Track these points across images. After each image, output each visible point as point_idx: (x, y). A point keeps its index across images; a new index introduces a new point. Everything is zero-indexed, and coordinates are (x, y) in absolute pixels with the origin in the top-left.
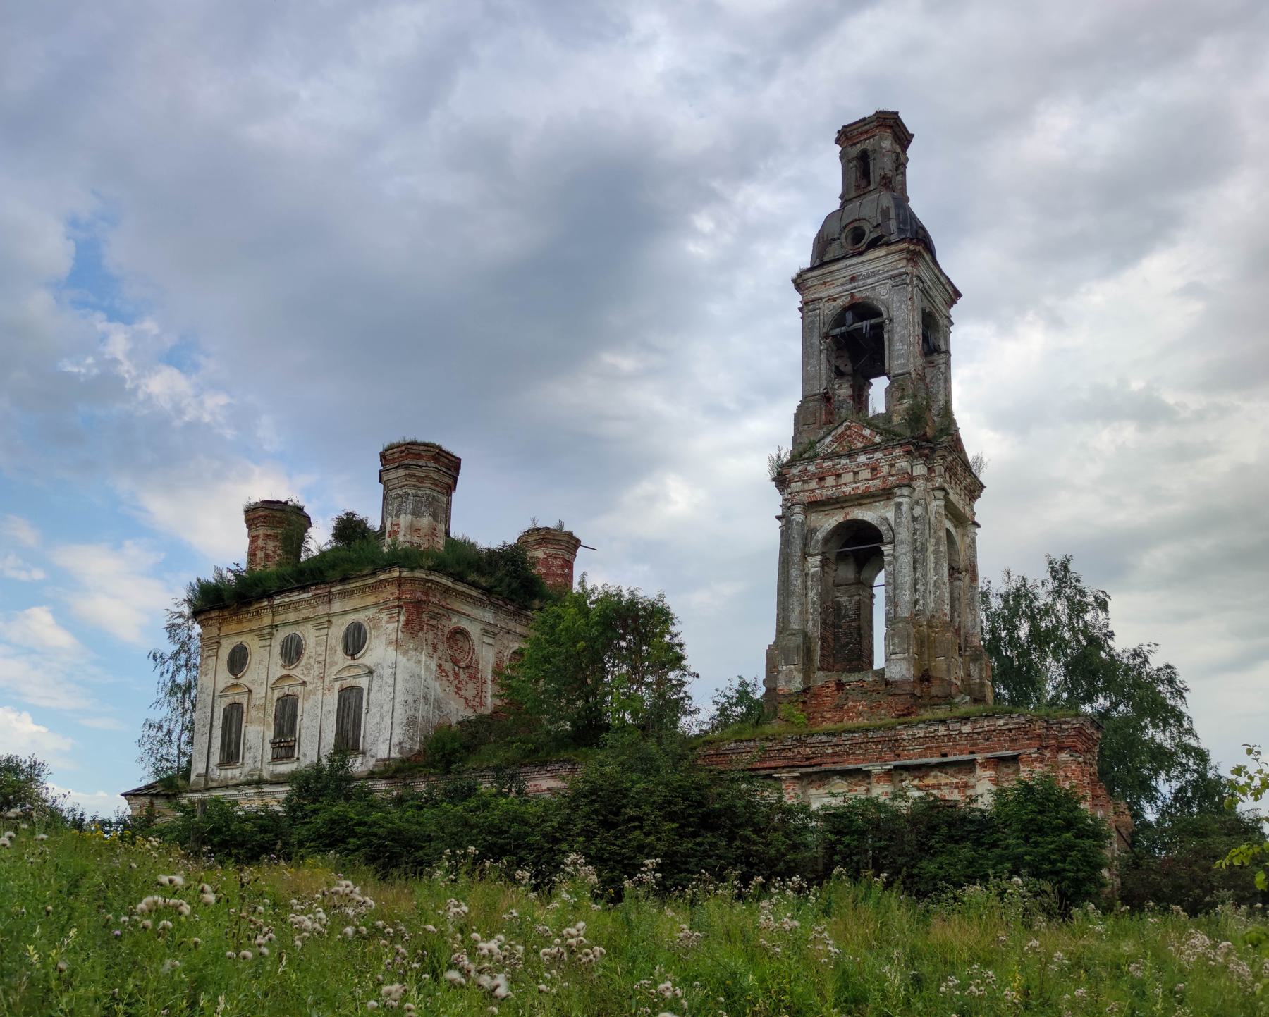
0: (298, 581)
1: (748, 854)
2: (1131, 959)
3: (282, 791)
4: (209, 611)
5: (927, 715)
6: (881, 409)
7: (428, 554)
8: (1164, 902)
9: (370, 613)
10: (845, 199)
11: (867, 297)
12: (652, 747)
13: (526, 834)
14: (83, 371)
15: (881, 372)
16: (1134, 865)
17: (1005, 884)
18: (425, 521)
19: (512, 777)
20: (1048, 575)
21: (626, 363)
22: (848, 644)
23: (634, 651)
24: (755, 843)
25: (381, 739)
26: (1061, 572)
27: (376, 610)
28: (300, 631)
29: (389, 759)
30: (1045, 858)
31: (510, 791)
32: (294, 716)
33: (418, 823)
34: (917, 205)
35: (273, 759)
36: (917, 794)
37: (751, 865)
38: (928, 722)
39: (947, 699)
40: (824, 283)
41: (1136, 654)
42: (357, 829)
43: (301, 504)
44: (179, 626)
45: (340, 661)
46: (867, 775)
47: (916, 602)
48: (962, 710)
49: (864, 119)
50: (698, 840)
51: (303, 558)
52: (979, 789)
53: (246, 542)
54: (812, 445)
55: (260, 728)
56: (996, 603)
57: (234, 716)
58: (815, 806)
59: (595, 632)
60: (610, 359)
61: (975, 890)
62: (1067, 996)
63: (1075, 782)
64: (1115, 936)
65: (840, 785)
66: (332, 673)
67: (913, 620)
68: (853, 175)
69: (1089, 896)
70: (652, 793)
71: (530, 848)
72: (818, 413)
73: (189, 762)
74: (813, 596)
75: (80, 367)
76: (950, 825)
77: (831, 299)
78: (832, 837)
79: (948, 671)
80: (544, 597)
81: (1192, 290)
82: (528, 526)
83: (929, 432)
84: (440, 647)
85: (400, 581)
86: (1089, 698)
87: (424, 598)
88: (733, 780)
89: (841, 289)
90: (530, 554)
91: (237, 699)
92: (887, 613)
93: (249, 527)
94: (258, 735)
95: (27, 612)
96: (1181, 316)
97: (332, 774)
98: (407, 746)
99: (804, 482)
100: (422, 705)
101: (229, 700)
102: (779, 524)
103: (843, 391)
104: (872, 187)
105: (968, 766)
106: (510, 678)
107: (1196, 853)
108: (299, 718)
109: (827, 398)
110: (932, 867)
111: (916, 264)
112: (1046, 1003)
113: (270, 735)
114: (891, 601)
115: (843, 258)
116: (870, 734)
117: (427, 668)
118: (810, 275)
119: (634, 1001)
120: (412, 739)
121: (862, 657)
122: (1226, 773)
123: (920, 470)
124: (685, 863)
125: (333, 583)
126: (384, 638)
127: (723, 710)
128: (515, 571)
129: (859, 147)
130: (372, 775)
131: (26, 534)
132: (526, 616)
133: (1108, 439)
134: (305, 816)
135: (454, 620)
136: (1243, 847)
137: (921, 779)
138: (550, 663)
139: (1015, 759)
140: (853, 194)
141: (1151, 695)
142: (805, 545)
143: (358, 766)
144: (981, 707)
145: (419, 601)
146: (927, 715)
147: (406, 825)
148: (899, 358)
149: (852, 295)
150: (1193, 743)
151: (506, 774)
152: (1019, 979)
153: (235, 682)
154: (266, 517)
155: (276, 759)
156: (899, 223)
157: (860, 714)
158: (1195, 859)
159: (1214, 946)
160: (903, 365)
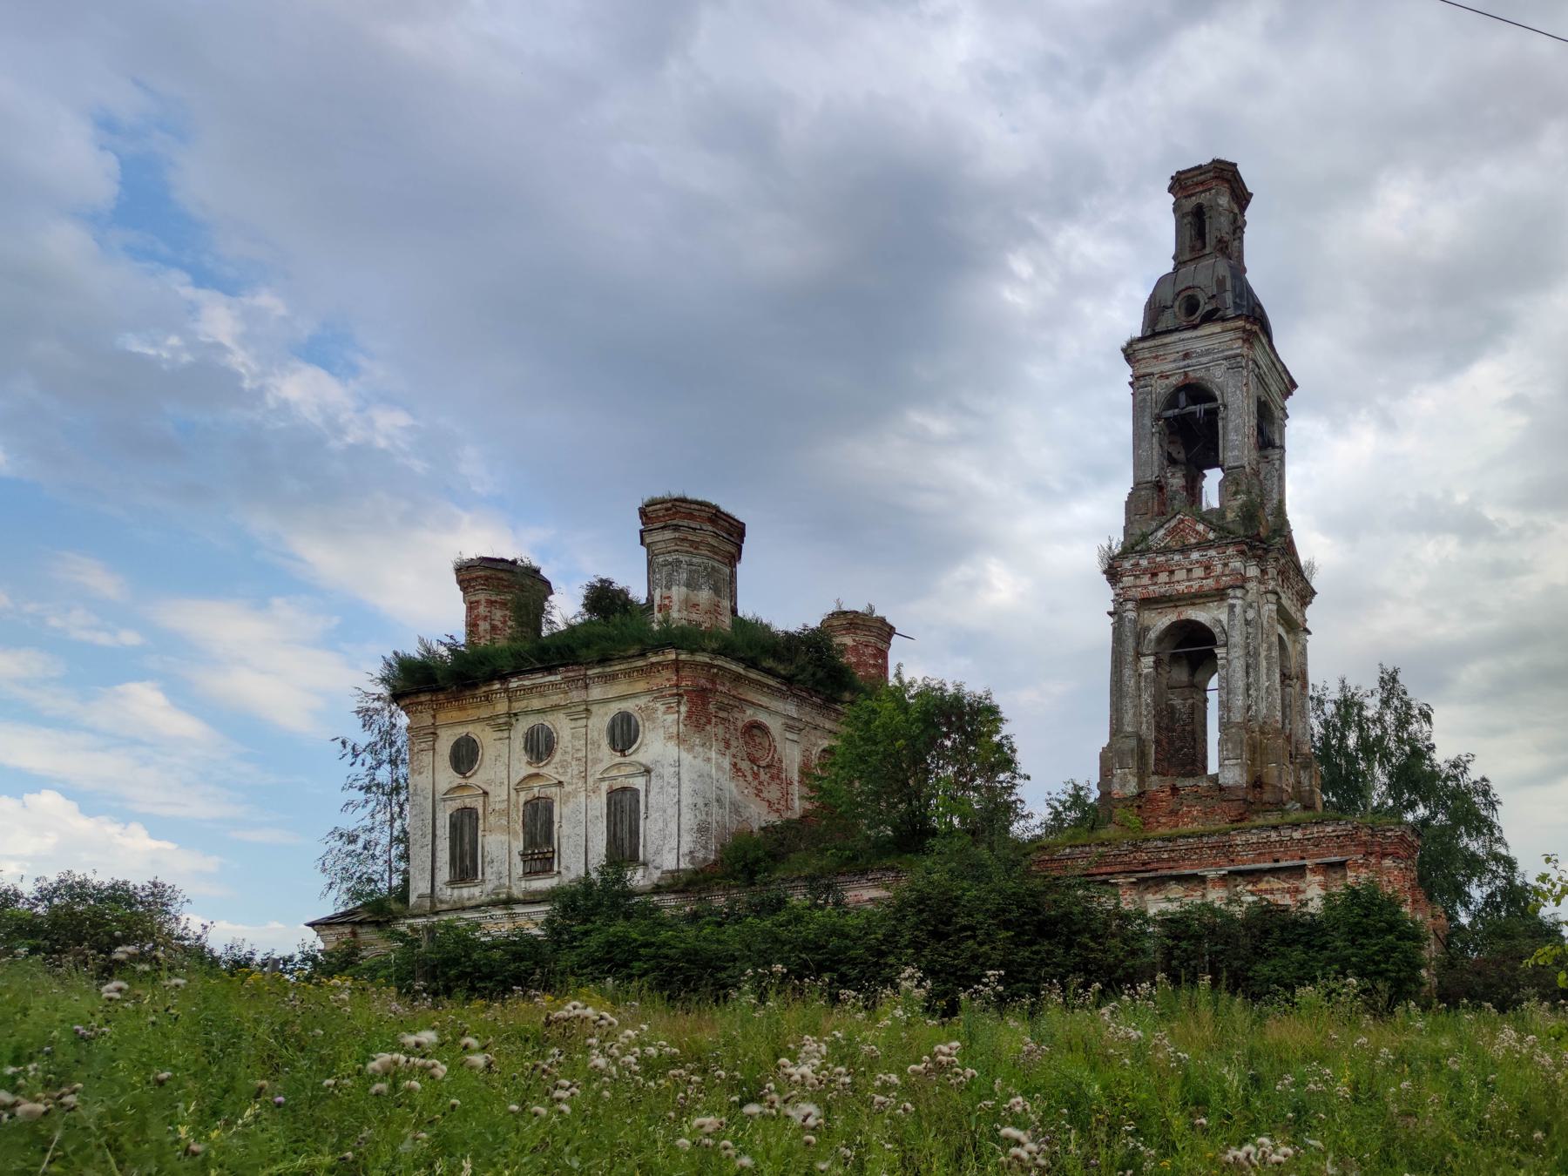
0: (541, 661)
1: (1086, 961)
2: (1450, 1053)
3: (541, 911)
4: (418, 692)
5: (1260, 821)
6: (1216, 505)
7: (710, 634)
8: (1476, 999)
9: (642, 701)
10: (1179, 261)
11: (1202, 378)
12: (983, 852)
13: (847, 948)
14: (165, 355)
15: (1214, 464)
16: (1449, 964)
17: (1333, 985)
18: (704, 596)
19: (828, 887)
20: (1376, 685)
21: (938, 426)
22: (1182, 748)
23: (959, 750)
24: (1092, 950)
25: (666, 848)
26: (1389, 683)
27: (649, 698)
28: (548, 721)
29: (678, 870)
30: (1370, 959)
31: (826, 902)
32: (550, 822)
33: (719, 942)
34: (1256, 277)
35: (525, 874)
36: (1251, 899)
37: (1088, 972)
38: (1260, 828)
39: (1279, 806)
40: (1156, 357)
41: (1455, 766)
42: (642, 951)
43: (535, 564)
44: (376, 711)
45: (606, 758)
46: (1202, 880)
47: (1249, 707)
48: (1293, 816)
49: (1200, 167)
50: (1035, 948)
51: (545, 632)
52: (1309, 894)
53: (462, 609)
54: (1144, 537)
55: (505, 838)
56: (1330, 708)
57: (464, 826)
58: (1152, 911)
59: (915, 730)
60: (917, 418)
61: (1306, 993)
62: (1393, 1090)
63: (1397, 887)
64: (1434, 1032)
65: (1176, 891)
66: (596, 771)
67: (1245, 726)
68: (1188, 233)
69: (1408, 995)
70: (984, 901)
71: (853, 962)
72: (1153, 503)
73: (406, 881)
74: (1146, 698)
75: (168, 349)
76: (1283, 929)
77: (1164, 376)
78: (1169, 942)
79: (1280, 777)
80: (856, 689)
81: (1518, 403)
82: (833, 608)
83: (1263, 532)
84: (734, 743)
85: (677, 666)
86: (1412, 806)
87: (709, 686)
88: (1069, 887)
89: (1173, 365)
90: (837, 640)
91: (468, 802)
92: (1221, 718)
93: (464, 589)
94: (501, 847)
95: (119, 688)
96: (1505, 429)
97: (605, 890)
98: (700, 855)
99: (1137, 577)
100: (715, 808)
101: (458, 804)
102: (1111, 620)
103: (1176, 481)
104: (1207, 251)
105: (1299, 871)
106: (820, 779)
107: (1505, 953)
108: (556, 826)
109: (1159, 487)
110: (1266, 970)
111: (1252, 347)
112: (1374, 1097)
113: (518, 845)
114: (1225, 706)
115: (1176, 330)
116: (1205, 839)
117: (719, 767)
118: (1141, 345)
119: (973, 1118)
120: (705, 848)
121: (1196, 762)
122: (1532, 880)
123: (1253, 571)
124: (1022, 972)
125: (590, 664)
126: (661, 731)
127: (1057, 815)
128: (820, 659)
129: (1194, 200)
130: (657, 889)
131: (102, 582)
132: (836, 710)
133: (1438, 551)
134: (574, 939)
135: (749, 712)
136: (1548, 948)
137: (1255, 884)
138: (866, 762)
139: (1342, 865)
140: (1187, 256)
141: (1468, 807)
142: (1138, 644)
143: (638, 879)
144: (1311, 813)
145: (704, 690)
146: (1260, 821)
147: (704, 945)
148: (1233, 449)
149: (1186, 374)
150: (1503, 851)
151: (821, 883)
152: (1348, 1075)
153: (463, 782)
154: (487, 578)
155: (529, 874)
156: (1235, 296)
157: (1194, 819)
158: (1503, 961)
159: (1521, 1040)
160: (1237, 458)
